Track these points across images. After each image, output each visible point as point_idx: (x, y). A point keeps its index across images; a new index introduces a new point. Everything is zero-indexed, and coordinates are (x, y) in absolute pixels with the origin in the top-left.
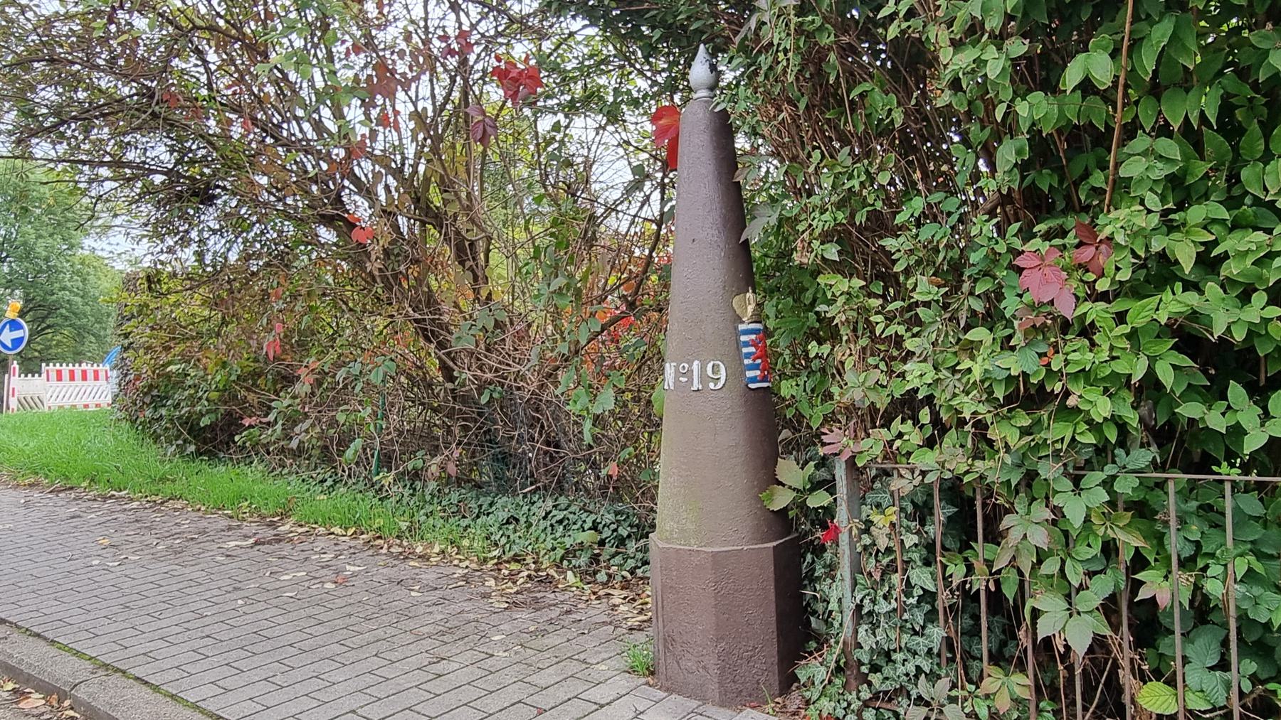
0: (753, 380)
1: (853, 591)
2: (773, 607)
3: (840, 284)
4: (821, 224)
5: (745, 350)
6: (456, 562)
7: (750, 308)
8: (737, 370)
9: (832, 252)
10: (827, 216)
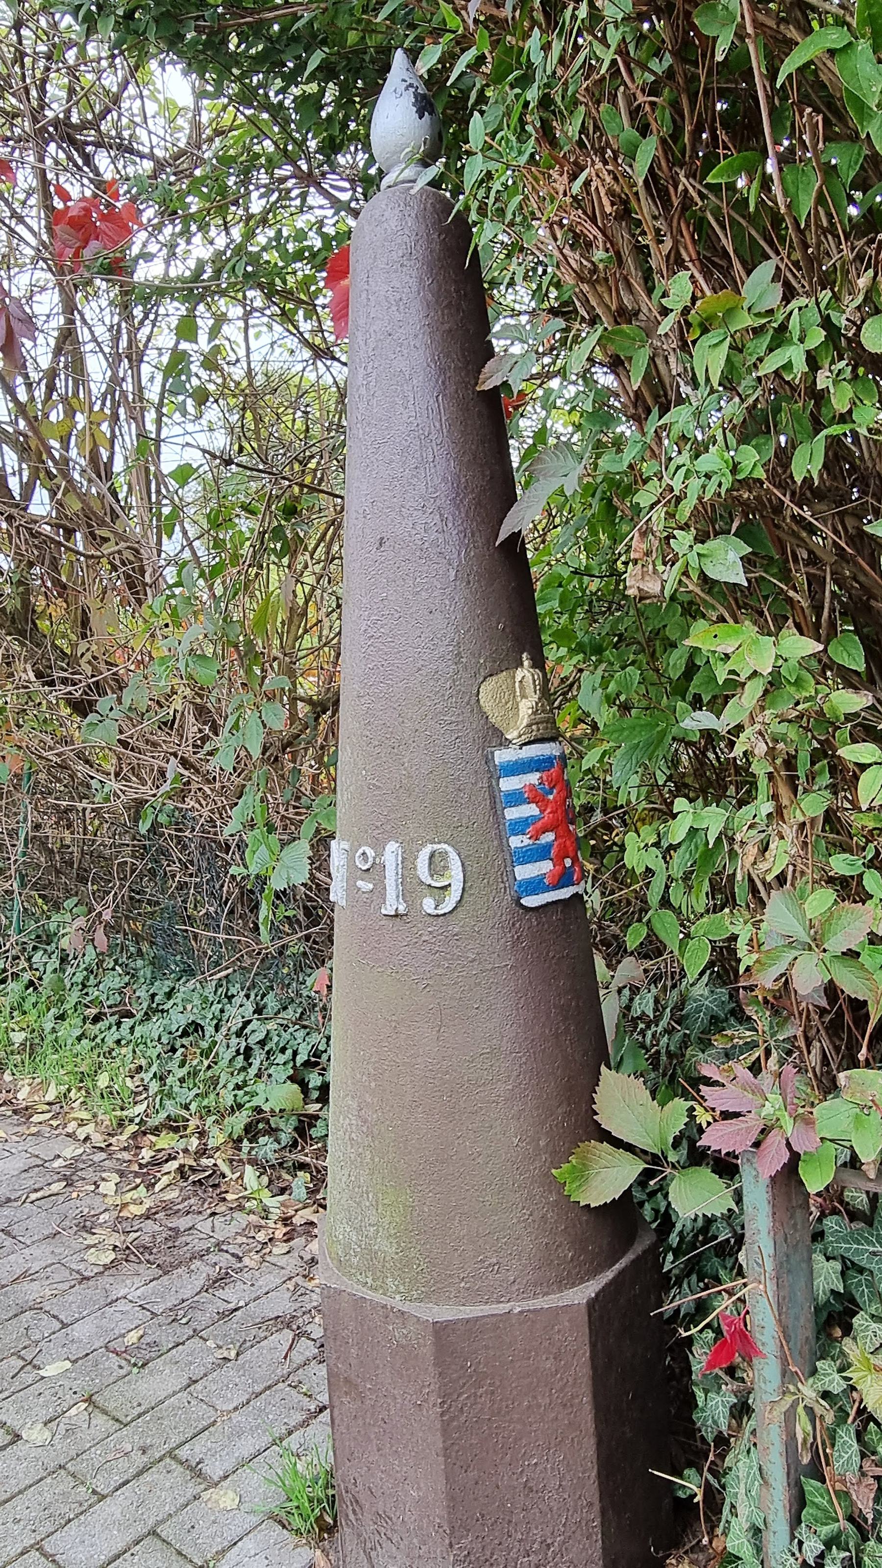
0: (535, 886)
1: (796, 1521)
2: (588, 1448)
3: (746, 650)
4: (695, 483)
5: (512, 814)
6: (72, 1127)
7: (526, 707)
8: (491, 864)
9: (727, 561)
10: (711, 460)
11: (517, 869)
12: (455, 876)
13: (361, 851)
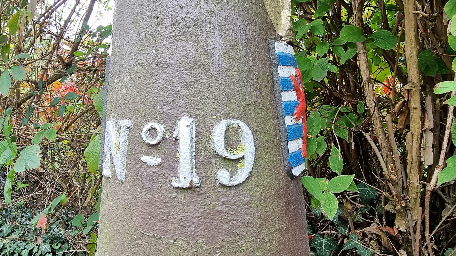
11: (290, 144)
12: (247, 147)
13: (148, 127)
